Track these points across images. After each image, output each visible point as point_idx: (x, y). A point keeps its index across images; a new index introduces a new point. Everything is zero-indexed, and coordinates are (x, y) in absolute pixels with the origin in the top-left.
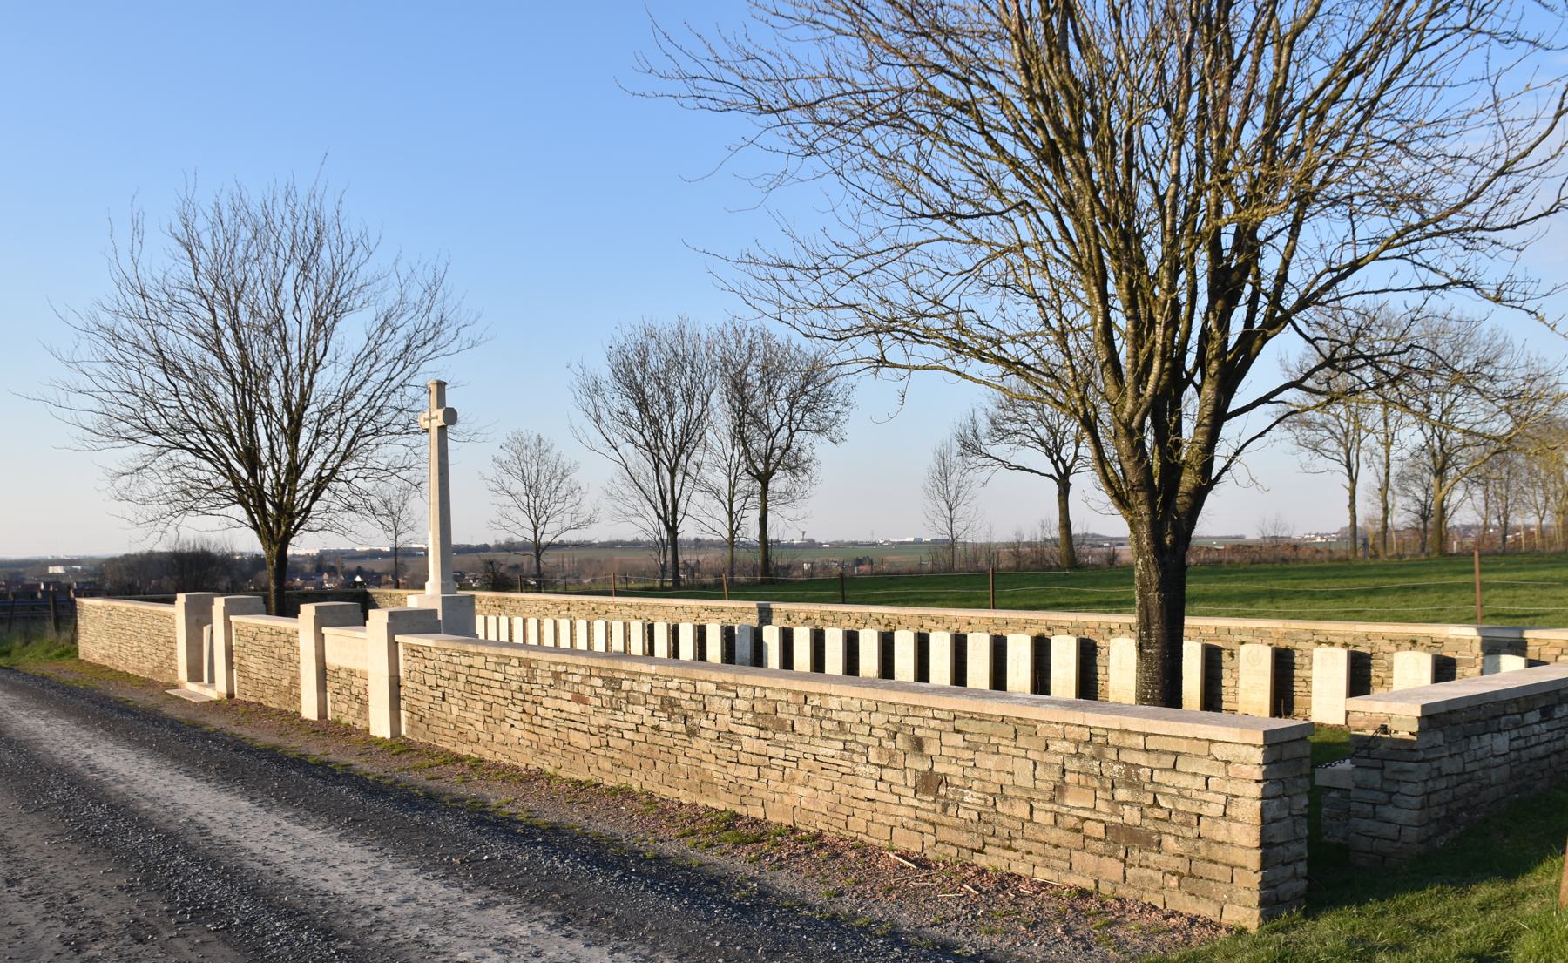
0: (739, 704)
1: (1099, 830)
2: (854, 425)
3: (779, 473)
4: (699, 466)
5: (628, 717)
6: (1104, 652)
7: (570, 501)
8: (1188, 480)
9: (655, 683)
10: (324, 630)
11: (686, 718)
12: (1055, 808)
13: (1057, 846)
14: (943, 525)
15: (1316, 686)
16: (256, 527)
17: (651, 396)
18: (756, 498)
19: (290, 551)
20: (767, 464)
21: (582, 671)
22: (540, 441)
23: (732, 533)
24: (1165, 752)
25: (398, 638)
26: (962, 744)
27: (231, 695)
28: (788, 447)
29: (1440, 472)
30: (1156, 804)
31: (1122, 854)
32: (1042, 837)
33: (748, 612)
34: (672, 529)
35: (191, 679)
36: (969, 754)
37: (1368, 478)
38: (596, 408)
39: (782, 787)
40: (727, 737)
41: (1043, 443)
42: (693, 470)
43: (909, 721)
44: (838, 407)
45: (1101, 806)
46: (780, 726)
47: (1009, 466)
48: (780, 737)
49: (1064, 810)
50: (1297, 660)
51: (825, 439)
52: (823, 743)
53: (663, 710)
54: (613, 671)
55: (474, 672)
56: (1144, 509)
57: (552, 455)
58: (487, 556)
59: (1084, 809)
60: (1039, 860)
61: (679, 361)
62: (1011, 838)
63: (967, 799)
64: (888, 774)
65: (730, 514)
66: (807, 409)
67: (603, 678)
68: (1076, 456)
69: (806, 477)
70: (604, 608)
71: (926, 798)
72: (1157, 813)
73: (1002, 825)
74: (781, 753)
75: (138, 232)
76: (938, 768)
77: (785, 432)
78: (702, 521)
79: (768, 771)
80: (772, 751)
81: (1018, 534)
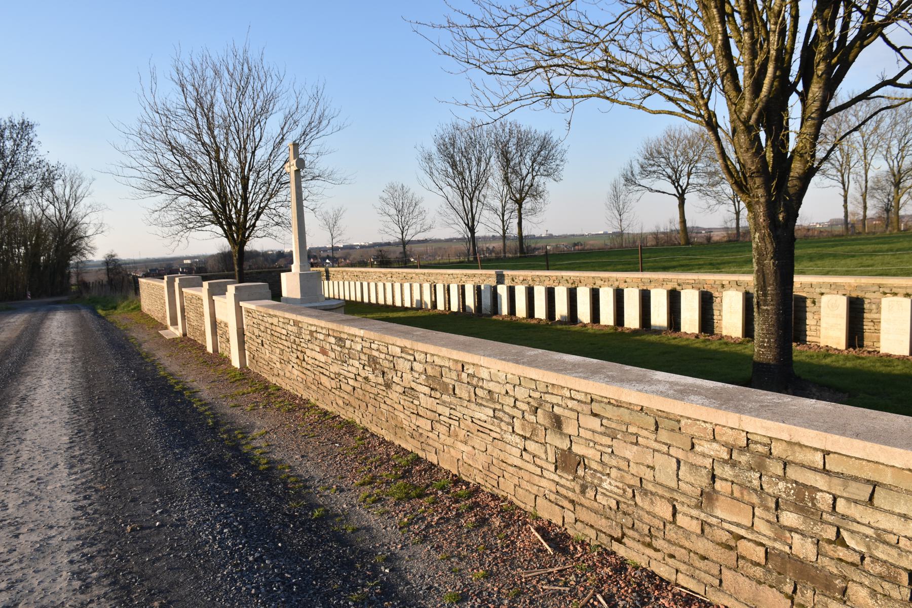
0: (416, 366)
1: (758, 554)
2: (567, 171)
3: (528, 199)
4: (484, 197)
5: (350, 368)
6: (718, 300)
7: (420, 217)
8: (797, 168)
9: (364, 344)
10: (214, 298)
11: (384, 373)
12: (703, 516)
13: (704, 558)
14: (616, 223)
15: (884, 326)
16: (227, 237)
17: (459, 161)
18: (516, 213)
19: (248, 248)
20: (521, 194)
21: (324, 331)
22: (403, 187)
23: (504, 233)
24: (856, 479)
25: (241, 304)
26: (599, 429)
27: (185, 335)
28: (532, 185)
29: (897, 185)
30: (839, 541)
31: (789, 589)
32: (687, 544)
33: (490, 276)
34: (472, 230)
35: (172, 325)
36: (606, 440)
37: (854, 191)
38: (430, 168)
39: (449, 441)
40: (409, 392)
41: (670, 177)
42: (482, 199)
43: (548, 398)
44: (558, 162)
45: (761, 526)
46: (444, 388)
47: (651, 190)
48: (445, 398)
49: (714, 521)
50: (866, 306)
51: (551, 180)
52: (477, 408)
53: (370, 366)
54: (340, 332)
55: (274, 328)
56: (760, 192)
57: (410, 195)
58: (439, 245)
59: (738, 525)
60: (683, 567)
61: (472, 143)
62: (650, 535)
63: (605, 485)
64: (531, 446)
65: (503, 221)
66: (541, 164)
67: (336, 338)
68: (688, 184)
69: (541, 200)
70: (410, 276)
71: (565, 475)
72: (841, 552)
73: (641, 521)
74: (447, 411)
75: (154, 78)
76: (576, 449)
77: (530, 177)
78: (488, 226)
79: (438, 425)
80: (440, 409)
81: (657, 227)
